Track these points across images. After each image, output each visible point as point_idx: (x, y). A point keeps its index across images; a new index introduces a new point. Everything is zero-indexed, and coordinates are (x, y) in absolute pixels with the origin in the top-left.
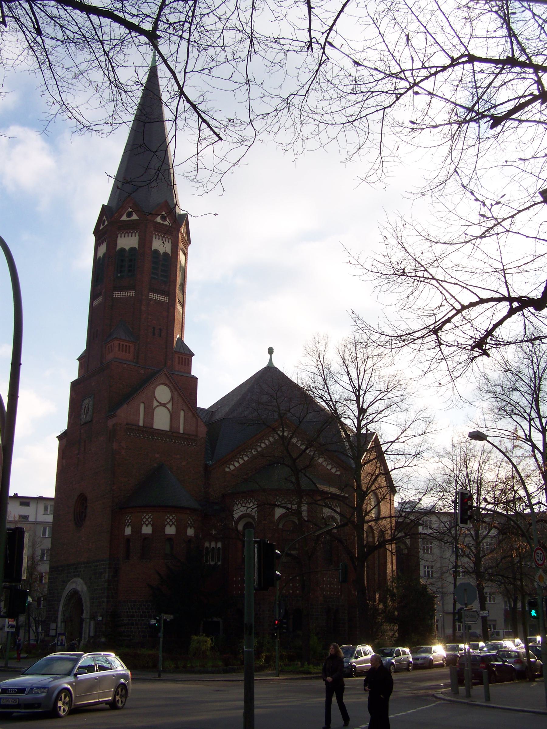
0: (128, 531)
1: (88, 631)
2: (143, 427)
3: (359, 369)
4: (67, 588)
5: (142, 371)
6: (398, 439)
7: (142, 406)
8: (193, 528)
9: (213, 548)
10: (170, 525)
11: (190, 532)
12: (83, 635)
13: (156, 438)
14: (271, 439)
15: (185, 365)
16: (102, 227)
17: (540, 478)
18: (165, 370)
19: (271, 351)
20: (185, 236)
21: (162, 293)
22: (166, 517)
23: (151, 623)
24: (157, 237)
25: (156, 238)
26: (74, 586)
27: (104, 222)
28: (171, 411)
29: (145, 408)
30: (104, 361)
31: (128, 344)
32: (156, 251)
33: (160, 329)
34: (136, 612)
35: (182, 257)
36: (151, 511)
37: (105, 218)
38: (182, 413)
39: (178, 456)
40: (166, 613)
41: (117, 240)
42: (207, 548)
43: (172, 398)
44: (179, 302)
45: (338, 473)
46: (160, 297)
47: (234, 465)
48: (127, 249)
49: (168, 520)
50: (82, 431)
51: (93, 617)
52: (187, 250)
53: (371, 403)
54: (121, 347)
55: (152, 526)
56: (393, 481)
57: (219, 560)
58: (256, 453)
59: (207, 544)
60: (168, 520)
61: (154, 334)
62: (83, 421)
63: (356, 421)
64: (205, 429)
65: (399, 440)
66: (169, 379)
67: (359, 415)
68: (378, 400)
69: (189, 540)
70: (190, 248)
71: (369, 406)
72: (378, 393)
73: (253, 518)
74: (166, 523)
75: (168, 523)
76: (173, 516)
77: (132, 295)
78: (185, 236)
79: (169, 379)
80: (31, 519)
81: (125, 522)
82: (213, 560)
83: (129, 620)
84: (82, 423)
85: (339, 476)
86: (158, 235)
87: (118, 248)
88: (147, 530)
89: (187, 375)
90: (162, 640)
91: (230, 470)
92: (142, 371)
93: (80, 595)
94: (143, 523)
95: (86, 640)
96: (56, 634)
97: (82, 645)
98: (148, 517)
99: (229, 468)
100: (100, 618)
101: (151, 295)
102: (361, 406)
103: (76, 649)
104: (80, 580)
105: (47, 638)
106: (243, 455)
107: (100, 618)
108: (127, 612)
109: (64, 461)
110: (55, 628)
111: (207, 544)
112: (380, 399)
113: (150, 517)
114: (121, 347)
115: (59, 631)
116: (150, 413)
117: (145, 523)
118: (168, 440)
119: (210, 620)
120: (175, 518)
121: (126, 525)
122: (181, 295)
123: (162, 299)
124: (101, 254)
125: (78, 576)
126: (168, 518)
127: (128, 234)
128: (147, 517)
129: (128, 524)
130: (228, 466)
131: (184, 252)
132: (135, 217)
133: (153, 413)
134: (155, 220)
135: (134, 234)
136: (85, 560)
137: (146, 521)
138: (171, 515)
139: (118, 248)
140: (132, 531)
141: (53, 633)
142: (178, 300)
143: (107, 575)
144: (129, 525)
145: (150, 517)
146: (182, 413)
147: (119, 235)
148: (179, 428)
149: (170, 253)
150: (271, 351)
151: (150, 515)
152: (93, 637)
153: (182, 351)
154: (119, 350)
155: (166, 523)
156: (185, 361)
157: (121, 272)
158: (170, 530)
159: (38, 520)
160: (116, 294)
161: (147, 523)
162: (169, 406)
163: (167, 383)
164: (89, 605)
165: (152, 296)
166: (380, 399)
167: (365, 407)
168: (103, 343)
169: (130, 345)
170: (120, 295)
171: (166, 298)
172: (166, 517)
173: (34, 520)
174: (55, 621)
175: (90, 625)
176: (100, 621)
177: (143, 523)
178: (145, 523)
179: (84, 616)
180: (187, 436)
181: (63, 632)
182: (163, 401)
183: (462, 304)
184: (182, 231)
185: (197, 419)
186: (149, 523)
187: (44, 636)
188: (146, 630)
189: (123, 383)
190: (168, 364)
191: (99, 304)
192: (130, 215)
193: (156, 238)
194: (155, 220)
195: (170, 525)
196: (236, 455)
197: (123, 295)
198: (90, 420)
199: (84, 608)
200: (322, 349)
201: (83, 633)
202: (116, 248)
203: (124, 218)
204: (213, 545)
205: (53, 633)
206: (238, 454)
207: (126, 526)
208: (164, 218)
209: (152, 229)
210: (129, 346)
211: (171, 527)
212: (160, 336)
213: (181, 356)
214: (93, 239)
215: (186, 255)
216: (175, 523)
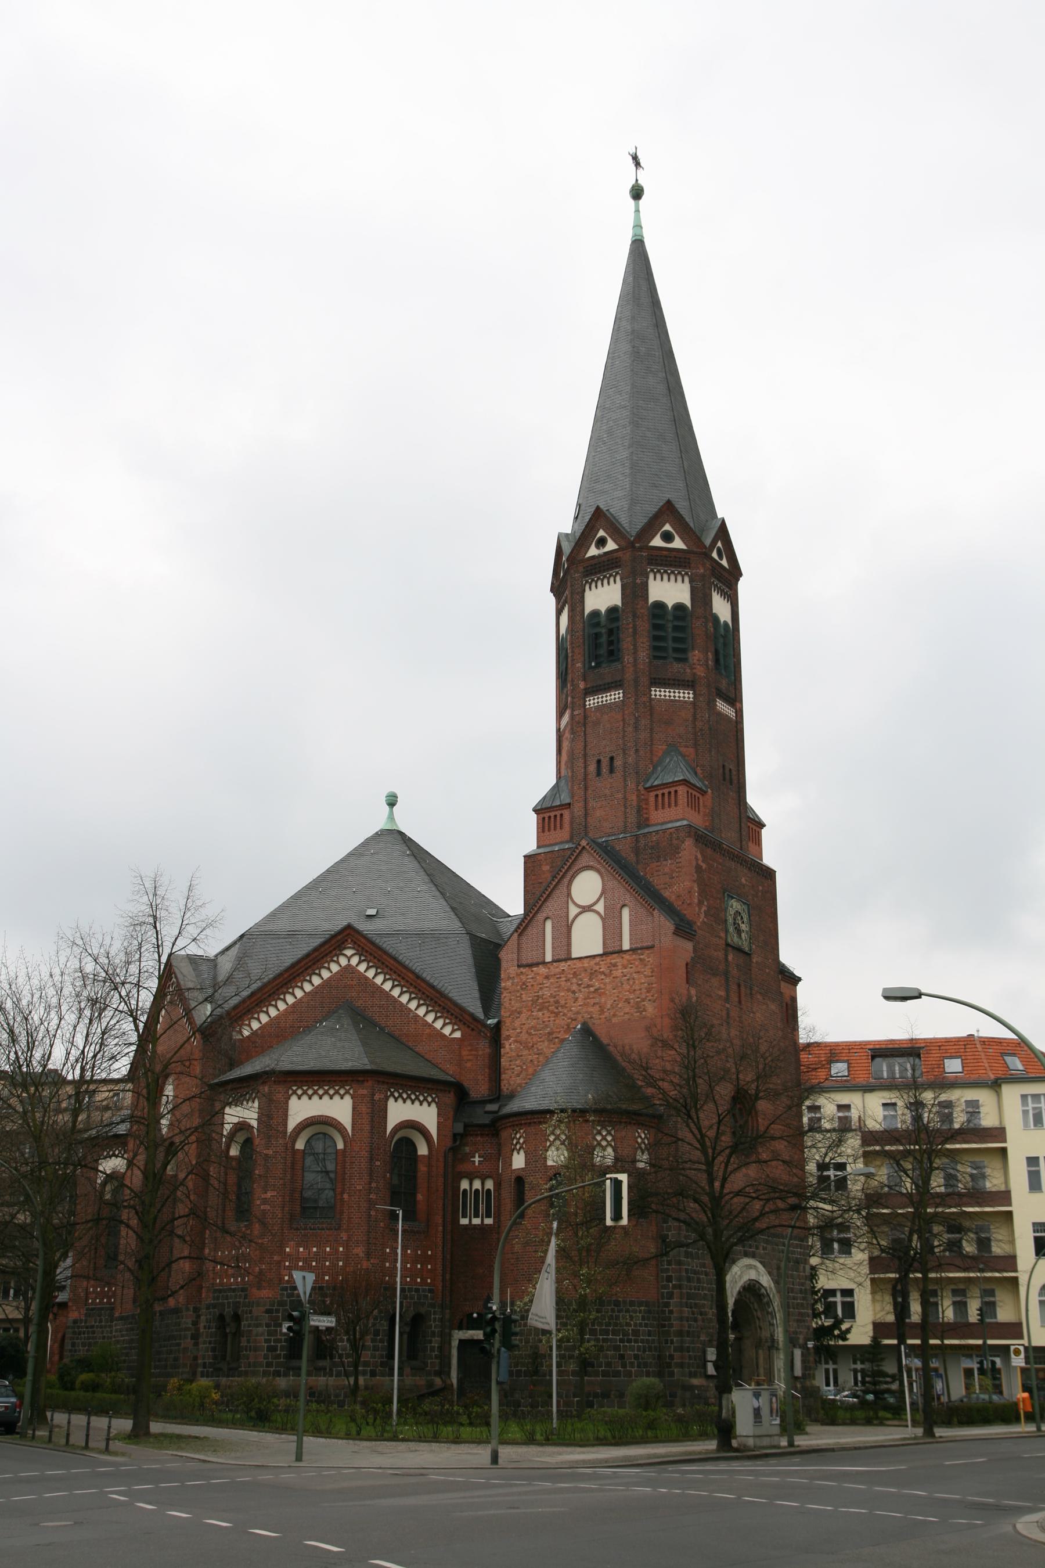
19: (392, 801)
32: (660, 605)
42: (465, 1191)
45: (458, 1035)
48: (670, 605)
81: (512, 1144)
101: (655, 691)
120: (613, 1132)
132: (678, 544)
140: (527, 1162)
147: (651, 576)
149: (688, 603)
150: (392, 801)
163: (595, 864)
192: (668, 537)
193: (655, 579)
204: (477, 1184)
207: (515, 1153)
208: (668, 537)
214: (552, 600)
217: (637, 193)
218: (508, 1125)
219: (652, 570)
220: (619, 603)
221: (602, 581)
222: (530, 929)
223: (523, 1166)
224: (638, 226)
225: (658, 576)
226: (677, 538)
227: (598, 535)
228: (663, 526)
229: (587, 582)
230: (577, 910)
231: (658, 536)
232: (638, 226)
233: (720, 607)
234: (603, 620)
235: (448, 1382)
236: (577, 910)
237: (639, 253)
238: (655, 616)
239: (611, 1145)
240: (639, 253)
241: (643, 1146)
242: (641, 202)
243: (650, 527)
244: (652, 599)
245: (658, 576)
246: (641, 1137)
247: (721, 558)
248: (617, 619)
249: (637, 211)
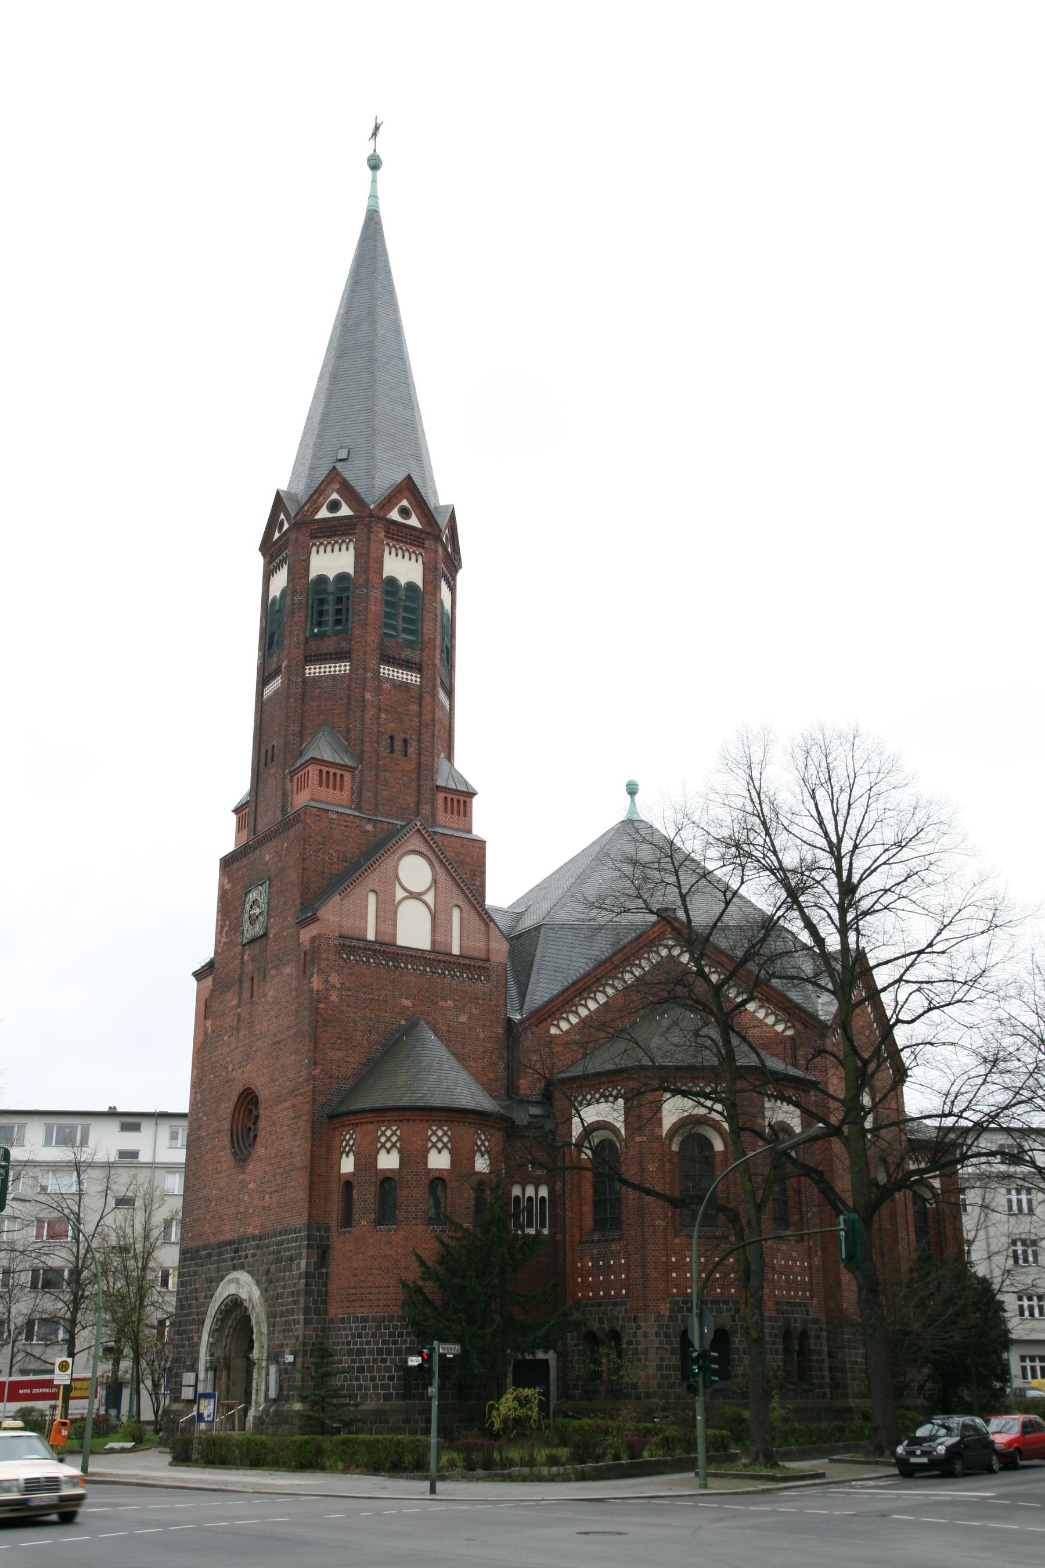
0: (348, 1165)
1: (263, 1388)
2: (376, 942)
3: (835, 801)
4: (217, 1294)
5: (369, 827)
6: (930, 945)
7: (372, 899)
8: (486, 1157)
9: (530, 1199)
10: (437, 1148)
11: (481, 1164)
12: (254, 1397)
13: (403, 965)
14: (610, 991)
15: (459, 814)
16: (277, 535)
18: (419, 824)
19: (632, 790)
20: (449, 549)
21: (407, 665)
22: (430, 1133)
23: (410, 1363)
24: (393, 551)
25: (390, 553)
26: (232, 1289)
27: (282, 524)
28: (433, 908)
29: (377, 902)
30: (289, 810)
31: (339, 772)
32: (392, 581)
33: (405, 741)
34: (368, 1343)
35: (445, 593)
36: (396, 1121)
37: (282, 516)
38: (456, 914)
39: (450, 1003)
40: (442, 1340)
41: (309, 558)
42: (517, 1198)
43: (435, 881)
44: (442, 683)
45: (789, 1033)
46: (403, 674)
47: (568, 1020)
48: (331, 576)
49: (434, 1139)
50: (246, 958)
51: (274, 1357)
52: (454, 579)
53: (865, 872)
54: (324, 778)
55: (400, 1152)
57: (543, 1225)
58: (577, 1020)
59: (516, 1191)
60: (434, 1139)
61: (392, 751)
62: (247, 936)
63: (835, 914)
64: (505, 946)
65: (935, 948)
66: (426, 841)
67: (842, 900)
68: (880, 866)
69: (481, 1183)
70: (460, 576)
71: (861, 880)
72: (879, 850)
73: (615, 1130)
74: (430, 1145)
75: (434, 1145)
76: (443, 1130)
77: (345, 670)
78: (449, 549)
79: (426, 841)
80: (144, 1157)
81: (342, 1146)
82: (530, 1225)
83: (353, 1361)
84: (245, 941)
85: (792, 1038)
88: (388, 1161)
89: (463, 835)
90: (435, 1403)
91: (562, 1030)
92: (369, 827)
93: (246, 1309)
94: (379, 1145)
95: (261, 1408)
96: (195, 1397)
97: (251, 1419)
98: (390, 1133)
99: (558, 1026)
100: (290, 1358)
101: (384, 669)
102: (845, 874)
104: (244, 1277)
105: (175, 1406)
106: (586, 999)
107: (290, 1358)
108: (348, 1343)
109: (209, 1023)
110: (193, 1383)
111: (516, 1191)
112: (884, 863)
113: (394, 1133)
114: (324, 778)
115: (201, 1389)
116: (388, 913)
117: (383, 1146)
118: (428, 969)
119: (531, 1357)
121: (344, 1151)
122: (444, 672)
123: (407, 679)
124: (276, 590)
125: (242, 1267)
126: (434, 1133)
127: (333, 546)
128: (388, 1133)
129: (347, 1149)
130: (555, 1022)
131: (448, 583)
132: (345, 511)
133: (396, 913)
134: (388, 516)
135: (344, 546)
136: (257, 1232)
137: (386, 1142)
138: (440, 1128)
140: (356, 1165)
141: (187, 1394)
142: (439, 680)
143: (303, 1263)
144: (349, 1151)
145: (394, 1133)
146: (456, 914)
147: (314, 549)
148: (451, 945)
149: (420, 583)
150: (632, 790)
151: (394, 1128)
152: (275, 1401)
153: (452, 785)
154: (321, 785)
155: (430, 1145)
156: (459, 806)
157: (320, 624)
158: (439, 1161)
159: (158, 1160)
160: (310, 669)
161: (388, 1145)
162: (430, 898)
163: (423, 849)
164: (265, 1331)
165: (388, 672)
166: (884, 863)
167: (855, 880)
168: (287, 771)
169: (344, 773)
170: (320, 672)
171: (416, 677)
172: (430, 1133)
173: (150, 1160)
174: (193, 1368)
175: (268, 1374)
176: (289, 1363)
177: (379, 1145)
178: (383, 1146)
179: (255, 1354)
180: (467, 962)
181: (209, 1390)
182: (416, 889)
184: (444, 539)
185: (487, 925)
186: (394, 1145)
187: (170, 1401)
189: (332, 851)
190: (424, 812)
191: (276, 692)
192: (334, 506)
193: (390, 553)
194: (388, 516)
195: (437, 1148)
196: (571, 1000)
197: (325, 672)
198: (261, 933)
199: (254, 1337)
200: (756, 758)
201: (254, 1392)
202: (308, 575)
203: (323, 513)
204: (530, 1191)
205: (187, 1394)
206: (576, 997)
207: (344, 1156)
208: (404, 512)
209: (382, 534)
210: (342, 776)
211: (440, 1152)
212: (406, 755)
213: (449, 796)
215: (453, 589)
216: (449, 1145)
217: (375, 164)
218: (347, 1123)
219: (388, 544)
220: (351, 570)
221: (340, 545)
222: (477, 918)
223: (352, 1170)
224: (374, 196)
226: (414, 516)
228: (400, 501)
229: (314, 544)
230: (403, 894)
232: (374, 196)
234: (331, 588)
236: (403, 894)
239: (447, 1147)
241: (483, 1149)
242: (379, 173)
243: (388, 502)
244: (386, 574)
246: (480, 1138)
247: (282, 521)
248: (347, 589)
249: (374, 181)
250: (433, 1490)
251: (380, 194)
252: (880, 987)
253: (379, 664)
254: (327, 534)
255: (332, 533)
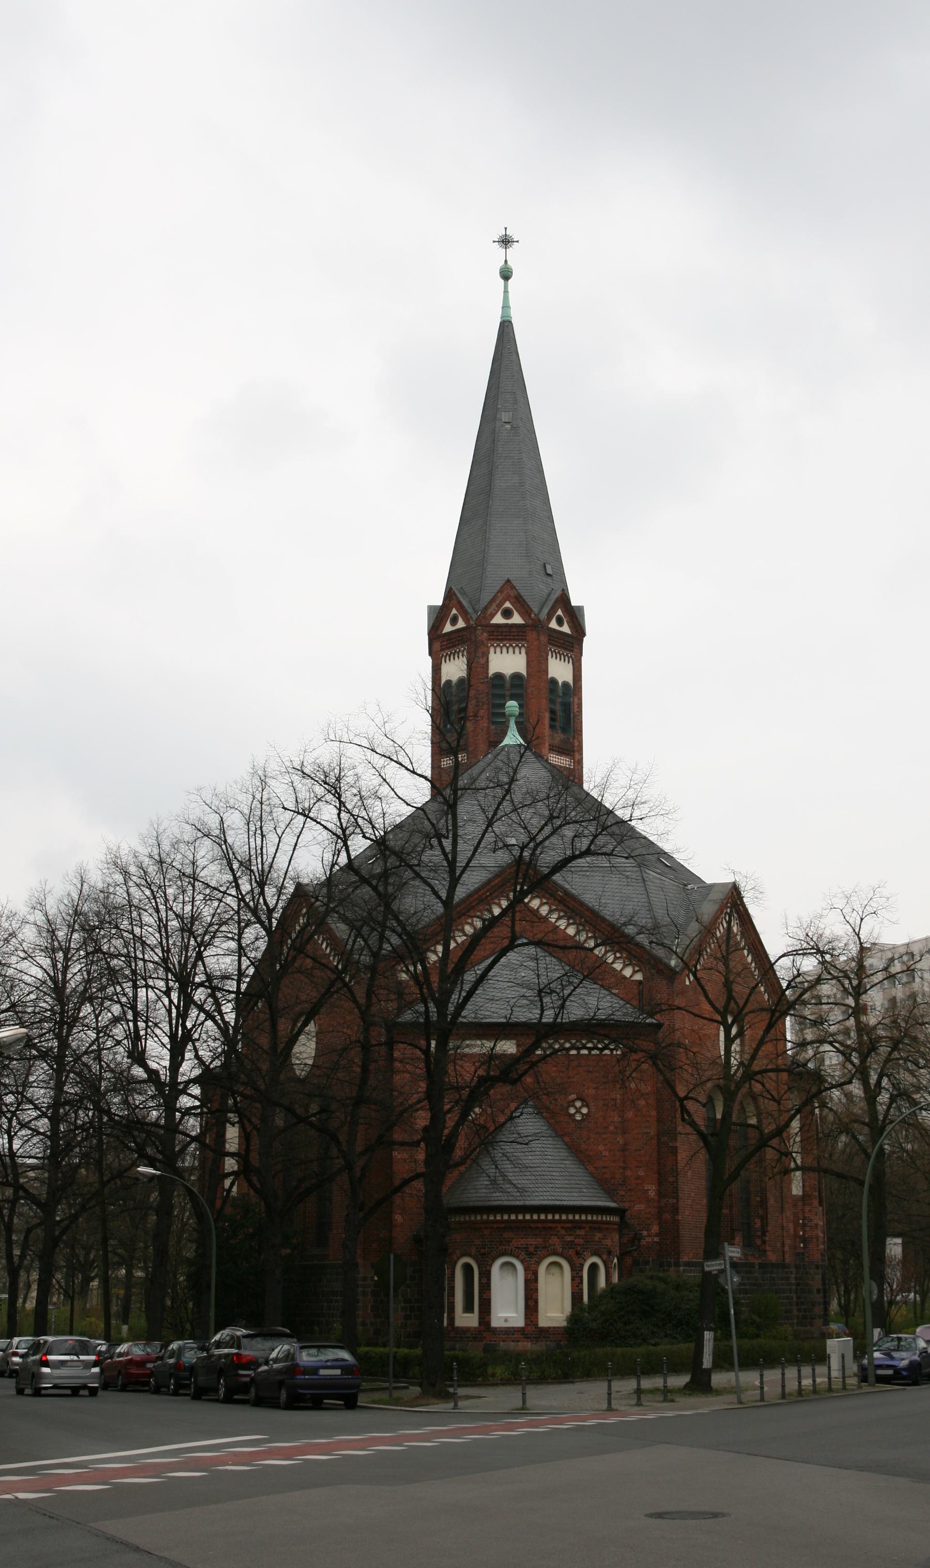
17: (171, 983)
25: (552, 657)
32: (554, 681)
45: (639, 977)
56: (471, 1000)
85: (640, 982)
86: (555, 651)
87: (491, 672)
103: (486, 1320)
132: (517, 619)
139: (491, 672)
147: (492, 650)
149: (524, 672)
183: (429, 660)
188: (378, 1320)
192: (507, 614)
193: (552, 657)
203: (498, 619)
208: (507, 614)
217: (506, 275)
219: (492, 645)
224: (506, 307)
225: (498, 649)
227: (452, 613)
231: (499, 613)
232: (506, 307)
233: (559, 670)
235: (308, 1396)
237: (506, 331)
238: (494, 686)
240: (506, 331)
245: (498, 649)
249: (506, 291)
250: (456, 1407)
251: (512, 303)
252: (773, 962)
253: (574, 769)
254: (500, 637)
255: (504, 637)
